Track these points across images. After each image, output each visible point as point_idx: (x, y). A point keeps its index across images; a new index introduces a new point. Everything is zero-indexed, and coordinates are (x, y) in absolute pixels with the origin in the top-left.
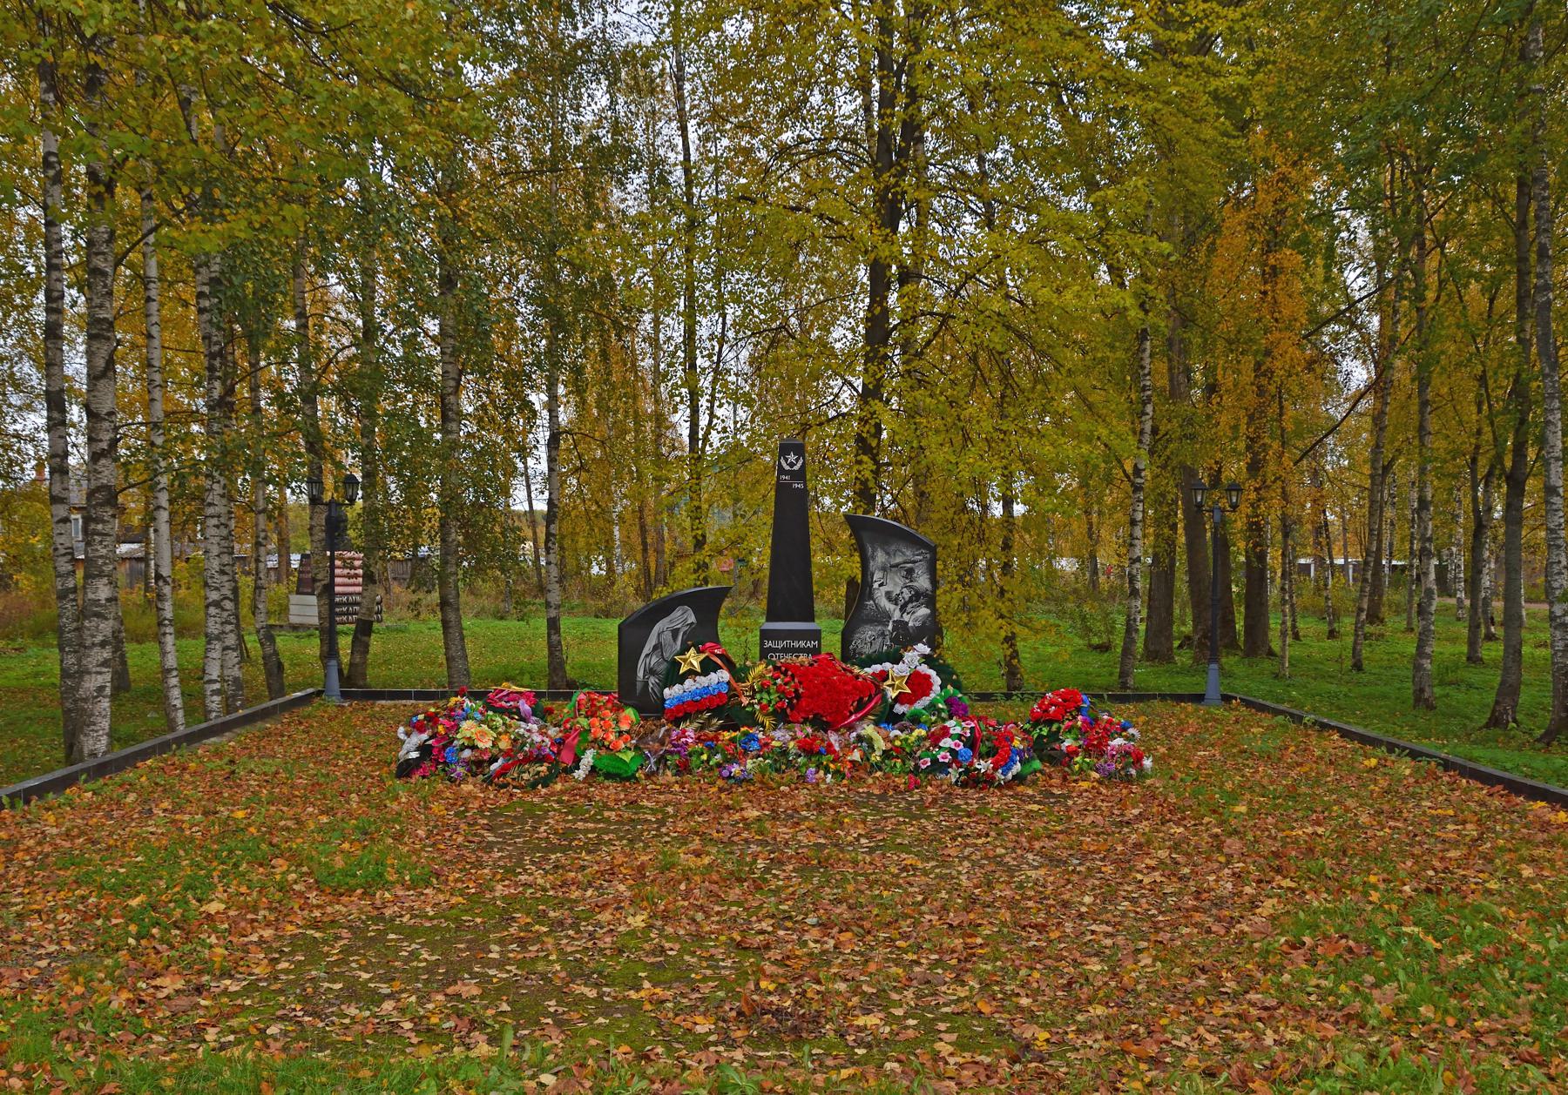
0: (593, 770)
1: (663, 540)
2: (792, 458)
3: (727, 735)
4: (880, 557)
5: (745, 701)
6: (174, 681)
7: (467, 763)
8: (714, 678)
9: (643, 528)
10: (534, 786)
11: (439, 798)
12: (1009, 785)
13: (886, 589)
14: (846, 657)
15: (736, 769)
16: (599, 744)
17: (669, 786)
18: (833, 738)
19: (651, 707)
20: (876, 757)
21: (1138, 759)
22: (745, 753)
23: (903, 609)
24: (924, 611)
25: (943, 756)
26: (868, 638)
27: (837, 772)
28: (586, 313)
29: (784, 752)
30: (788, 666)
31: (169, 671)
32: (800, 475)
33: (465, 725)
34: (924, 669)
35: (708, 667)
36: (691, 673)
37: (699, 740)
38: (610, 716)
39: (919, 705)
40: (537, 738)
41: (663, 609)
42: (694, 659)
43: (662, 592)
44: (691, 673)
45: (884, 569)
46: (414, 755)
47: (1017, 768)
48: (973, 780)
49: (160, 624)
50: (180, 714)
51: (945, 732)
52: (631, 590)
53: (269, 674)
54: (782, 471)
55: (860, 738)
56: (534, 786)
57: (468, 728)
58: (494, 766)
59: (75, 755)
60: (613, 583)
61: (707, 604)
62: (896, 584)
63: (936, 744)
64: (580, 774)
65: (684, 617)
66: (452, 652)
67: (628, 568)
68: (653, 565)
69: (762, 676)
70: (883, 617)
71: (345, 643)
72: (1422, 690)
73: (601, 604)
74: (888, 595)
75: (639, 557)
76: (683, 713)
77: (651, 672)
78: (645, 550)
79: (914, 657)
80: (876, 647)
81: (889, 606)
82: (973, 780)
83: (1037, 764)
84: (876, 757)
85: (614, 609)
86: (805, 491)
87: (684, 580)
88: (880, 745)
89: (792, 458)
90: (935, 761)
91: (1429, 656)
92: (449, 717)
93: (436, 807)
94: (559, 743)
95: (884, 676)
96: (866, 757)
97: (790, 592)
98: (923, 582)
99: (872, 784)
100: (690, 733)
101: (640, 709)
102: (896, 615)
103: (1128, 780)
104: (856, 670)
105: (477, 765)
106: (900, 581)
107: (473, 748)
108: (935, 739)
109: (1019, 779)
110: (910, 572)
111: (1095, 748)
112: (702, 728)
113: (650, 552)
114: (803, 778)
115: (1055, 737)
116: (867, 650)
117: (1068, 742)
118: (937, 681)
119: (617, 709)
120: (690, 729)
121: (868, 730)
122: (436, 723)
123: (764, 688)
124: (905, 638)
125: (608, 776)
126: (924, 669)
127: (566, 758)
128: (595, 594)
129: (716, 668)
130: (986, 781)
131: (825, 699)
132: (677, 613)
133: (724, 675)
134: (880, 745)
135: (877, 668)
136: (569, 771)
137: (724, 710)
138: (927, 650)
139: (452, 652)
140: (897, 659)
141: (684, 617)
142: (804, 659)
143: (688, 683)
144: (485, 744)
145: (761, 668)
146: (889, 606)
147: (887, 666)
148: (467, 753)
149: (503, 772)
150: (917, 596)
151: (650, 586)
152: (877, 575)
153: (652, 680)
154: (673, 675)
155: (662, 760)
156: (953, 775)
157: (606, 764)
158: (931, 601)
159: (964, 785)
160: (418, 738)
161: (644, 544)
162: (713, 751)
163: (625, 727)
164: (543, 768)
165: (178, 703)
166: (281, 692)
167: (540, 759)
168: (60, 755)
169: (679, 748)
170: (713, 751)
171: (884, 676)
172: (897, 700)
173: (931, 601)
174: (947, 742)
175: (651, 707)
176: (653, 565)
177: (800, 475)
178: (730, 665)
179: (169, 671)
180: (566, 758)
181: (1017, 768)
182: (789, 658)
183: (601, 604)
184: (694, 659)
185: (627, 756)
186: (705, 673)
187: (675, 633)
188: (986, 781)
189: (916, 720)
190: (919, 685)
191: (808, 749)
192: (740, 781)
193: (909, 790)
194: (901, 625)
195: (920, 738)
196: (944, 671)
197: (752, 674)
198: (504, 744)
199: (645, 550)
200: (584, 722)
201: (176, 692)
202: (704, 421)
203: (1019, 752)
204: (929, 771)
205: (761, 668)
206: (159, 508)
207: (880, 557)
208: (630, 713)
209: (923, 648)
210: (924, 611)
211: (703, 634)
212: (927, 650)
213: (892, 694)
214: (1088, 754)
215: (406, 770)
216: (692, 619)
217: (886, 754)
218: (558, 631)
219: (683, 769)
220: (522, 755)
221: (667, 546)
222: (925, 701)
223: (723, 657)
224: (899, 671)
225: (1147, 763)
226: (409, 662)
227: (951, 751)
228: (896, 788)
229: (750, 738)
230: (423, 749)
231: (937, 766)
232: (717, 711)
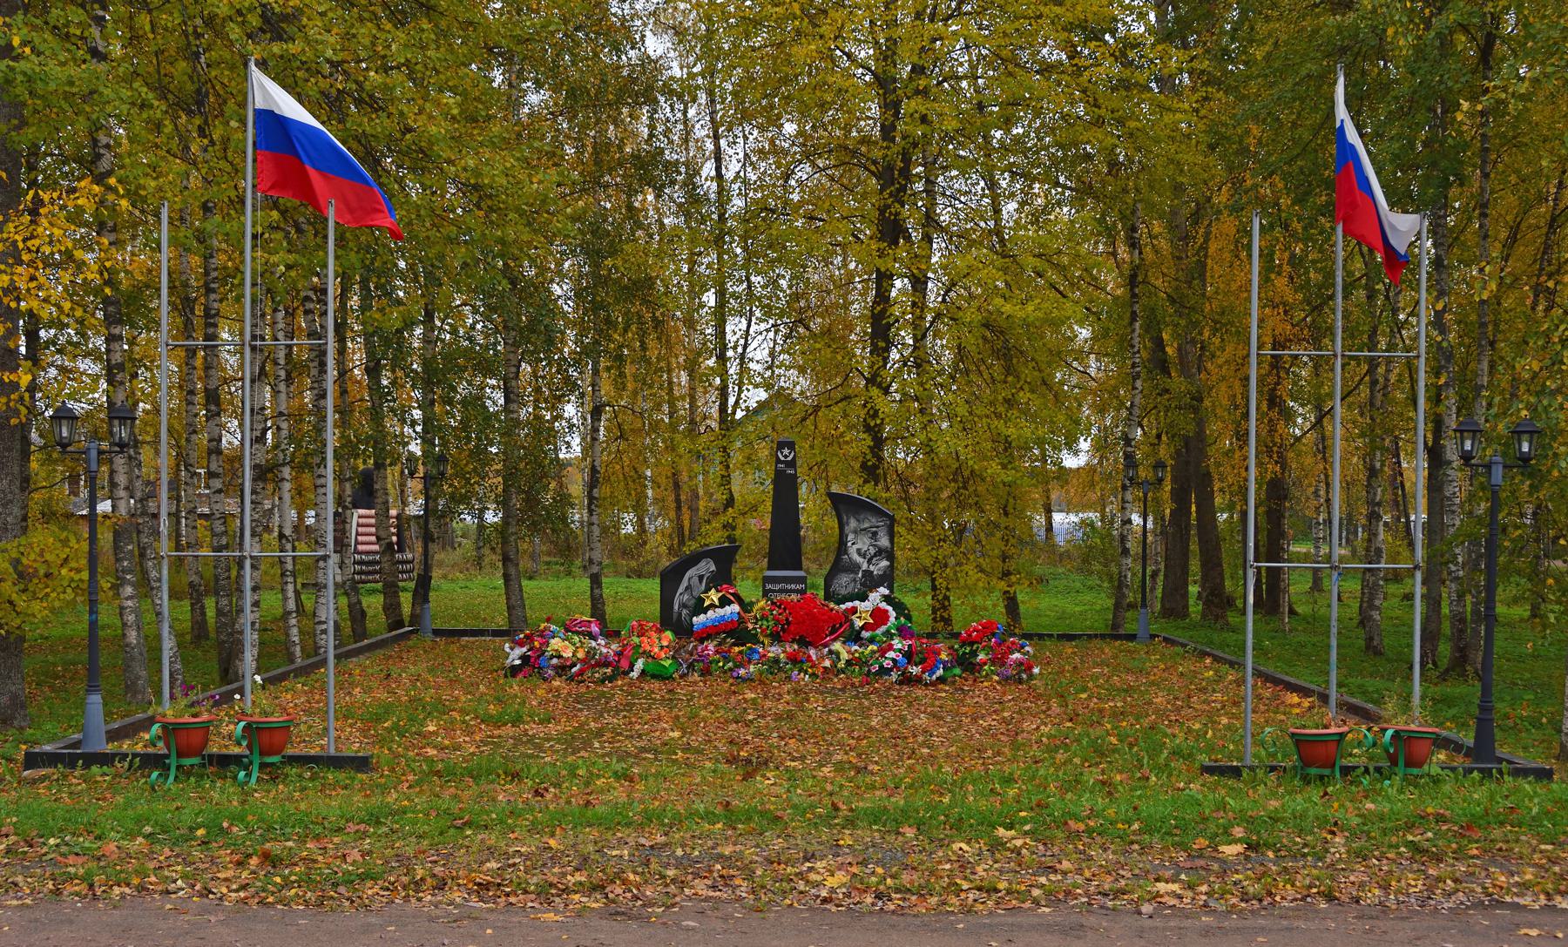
0: (643, 672)
1: (697, 497)
2: (786, 451)
3: (737, 649)
4: (853, 523)
5: (750, 626)
6: (293, 622)
7: (555, 667)
8: (728, 609)
9: (677, 486)
10: (603, 682)
11: (537, 694)
12: (933, 684)
13: (858, 546)
14: (828, 597)
15: (742, 672)
16: (647, 655)
17: (695, 683)
18: (812, 652)
19: (683, 630)
20: (841, 665)
21: (1030, 668)
22: (750, 662)
23: (869, 562)
24: (885, 563)
25: (887, 664)
26: (844, 583)
27: (813, 675)
28: (627, 307)
29: (776, 661)
30: (782, 602)
31: (290, 613)
32: (792, 464)
33: (553, 641)
34: (884, 605)
35: (724, 602)
36: (712, 606)
37: (717, 652)
38: (655, 636)
39: (879, 631)
40: (604, 650)
41: (694, 560)
42: (714, 596)
43: (691, 547)
44: (712, 606)
45: (855, 532)
46: (518, 662)
47: (940, 672)
48: (907, 680)
49: (283, 575)
50: (298, 648)
51: (890, 648)
52: (663, 549)
53: (353, 619)
54: (778, 461)
55: (831, 652)
56: (603, 682)
57: (555, 643)
58: (574, 670)
59: (231, 676)
60: (645, 543)
61: (725, 558)
62: (864, 543)
63: (883, 656)
64: (634, 674)
65: (707, 567)
66: (513, 601)
67: (659, 525)
68: (686, 523)
69: (762, 609)
70: (855, 568)
71: (406, 600)
72: (1371, 639)
73: (634, 564)
74: (858, 551)
75: (672, 514)
76: (708, 633)
77: (684, 606)
78: (679, 508)
79: (876, 598)
80: (850, 589)
81: (859, 559)
82: (907, 680)
83: (957, 671)
84: (841, 665)
85: (647, 569)
86: (795, 477)
87: (714, 537)
88: (845, 656)
89: (786, 451)
90: (881, 667)
91: (1378, 608)
92: (542, 636)
93: (539, 692)
94: (619, 654)
95: (854, 610)
96: (834, 665)
97: (785, 546)
98: (884, 542)
99: (837, 682)
100: (711, 647)
101: (676, 633)
102: (865, 566)
103: (1020, 681)
104: (832, 605)
105: (562, 669)
106: (867, 541)
107: (560, 657)
108: (883, 652)
109: (941, 680)
110: (875, 534)
111: (999, 660)
112: (720, 644)
113: (684, 509)
114: (789, 678)
115: (974, 654)
116: (843, 592)
117: (982, 656)
118: (893, 614)
119: (660, 631)
120: (711, 646)
121: (837, 646)
122: (533, 641)
123: (764, 617)
124: (871, 582)
125: (654, 676)
126: (884, 605)
127: (624, 664)
128: (626, 553)
129: (730, 603)
130: (916, 681)
131: (807, 627)
132: (703, 563)
133: (736, 608)
134: (845, 656)
135: (849, 605)
136: (626, 673)
137: (735, 632)
138: (887, 592)
139: (513, 601)
140: (864, 598)
141: (707, 567)
142: (794, 597)
143: (710, 613)
144: (568, 654)
145: (762, 603)
146: (859, 559)
147: (857, 603)
148: (555, 661)
149: (581, 672)
150: (880, 552)
151: (682, 543)
152: (851, 537)
153: (685, 611)
154: (700, 608)
155: (691, 666)
156: (894, 676)
157: (651, 668)
158: (890, 556)
159: (901, 683)
160: (519, 651)
161: (678, 501)
162: (726, 660)
163: (665, 643)
164: (609, 670)
165: (296, 639)
166: (364, 636)
167: (607, 664)
168: (216, 676)
169: (703, 658)
170: (726, 660)
171: (854, 610)
172: (863, 628)
173: (890, 556)
174: (891, 654)
175: (683, 630)
176: (686, 523)
177: (792, 464)
178: (740, 601)
179: (290, 613)
180: (624, 664)
181: (940, 672)
182: (783, 596)
183: (634, 564)
184: (714, 596)
185: (667, 663)
186: (722, 606)
187: (701, 578)
188: (916, 681)
189: (872, 641)
190: (879, 616)
191: (794, 659)
192: (744, 680)
193: (862, 686)
194: (868, 573)
195: (873, 652)
196: (900, 607)
197: (756, 607)
198: (581, 655)
199: (679, 508)
200: (636, 640)
201: (295, 631)
202: (732, 400)
203: (945, 663)
204: (877, 673)
205: (762, 603)
206: (283, 479)
207: (853, 523)
208: (669, 634)
209: (884, 591)
210: (885, 563)
211: (722, 578)
212: (887, 592)
213: (859, 623)
214: (993, 664)
215: (514, 671)
216: (713, 568)
217: (848, 663)
218: (600, 586)
219: (706, 672)
220: (593, 662)
221: (702, 504)
222: (884, 628)
223: (736, 595)
224: (865, 607)
225: (1036, 670)
226: (454, 617)
227: (894, 660)
228: (853, 685)
229: (754, 651)
230: (523, 657)
231: (884, 671)
232: (730, 633)
